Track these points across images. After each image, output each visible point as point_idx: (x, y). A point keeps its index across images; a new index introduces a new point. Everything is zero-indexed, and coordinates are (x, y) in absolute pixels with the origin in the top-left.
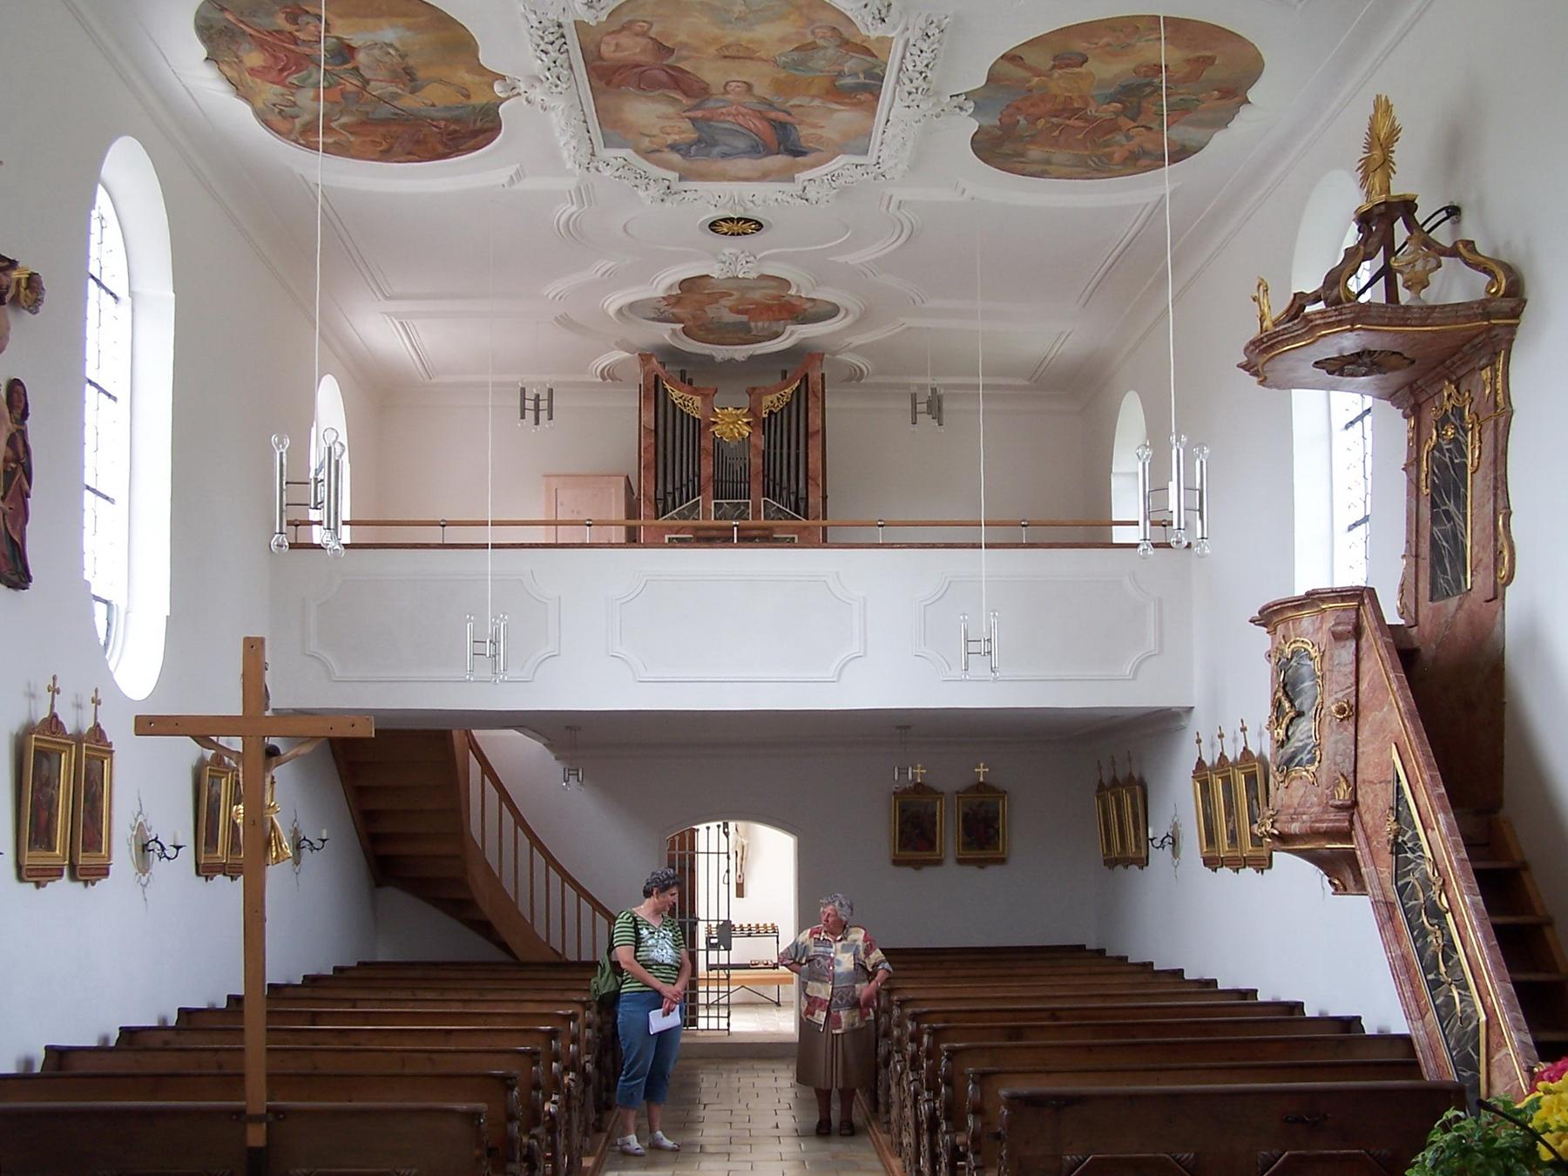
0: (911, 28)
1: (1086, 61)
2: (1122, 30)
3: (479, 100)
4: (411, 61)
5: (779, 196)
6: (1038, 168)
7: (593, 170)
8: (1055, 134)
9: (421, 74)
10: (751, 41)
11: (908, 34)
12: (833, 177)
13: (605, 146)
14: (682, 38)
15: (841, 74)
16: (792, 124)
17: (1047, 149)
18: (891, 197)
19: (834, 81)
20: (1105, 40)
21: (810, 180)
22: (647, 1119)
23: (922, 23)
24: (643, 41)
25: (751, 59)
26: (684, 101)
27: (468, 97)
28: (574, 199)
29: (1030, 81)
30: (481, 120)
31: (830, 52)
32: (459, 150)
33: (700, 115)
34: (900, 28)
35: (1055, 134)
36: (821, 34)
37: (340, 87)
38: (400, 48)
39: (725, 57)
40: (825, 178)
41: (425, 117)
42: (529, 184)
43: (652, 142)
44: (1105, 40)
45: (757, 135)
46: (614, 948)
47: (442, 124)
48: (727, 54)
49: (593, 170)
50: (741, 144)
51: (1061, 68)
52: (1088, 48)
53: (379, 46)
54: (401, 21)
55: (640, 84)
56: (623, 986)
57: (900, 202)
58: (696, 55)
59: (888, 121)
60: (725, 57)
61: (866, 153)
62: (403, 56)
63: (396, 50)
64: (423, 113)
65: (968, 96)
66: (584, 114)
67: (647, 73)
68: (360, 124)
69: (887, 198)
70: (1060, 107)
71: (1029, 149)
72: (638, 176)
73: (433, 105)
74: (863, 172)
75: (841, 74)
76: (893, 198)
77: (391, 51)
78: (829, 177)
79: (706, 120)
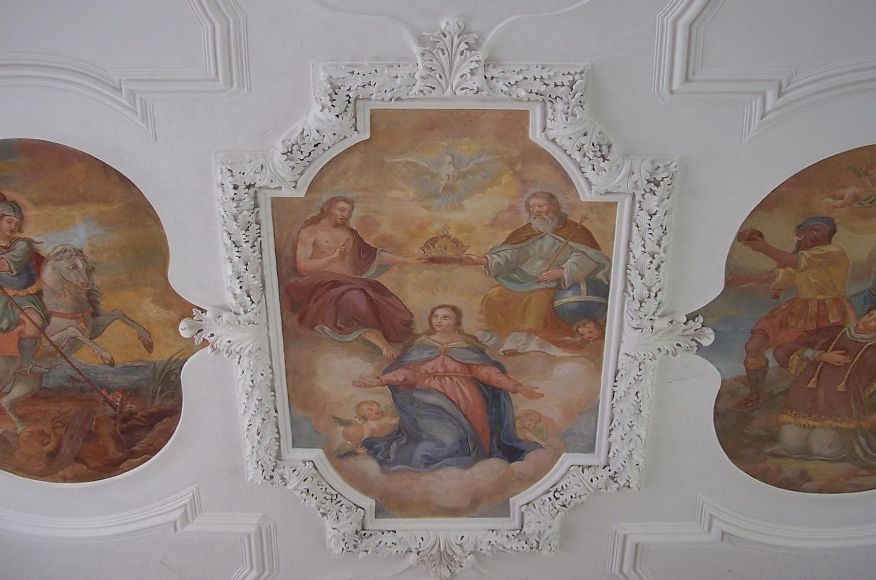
0: (636, 171)
1: (833, 231)
2: (866, 173)
3: (161, 355)
4: (98, 280)
5: (492, 537)
6: (791, 468)
7: (277, 478)
8: (811, 385)
9: (106, 304)
10: (461, 228)
11: (634, 177)
12: (555, 491)
13: (293, 447)
14: (385, 228)
15: (559, 286)
16: (506, 392)
17: (804, 422)
18: (625, 537)
19: (552, 301)
20: (852, 190)
21: (528, 504)
22: (53, 341)
23: (647, 166)
24: (342, 236)
25: (460, 261)
26: (384, 350)
27: (149, 347)
28: (255, 563)
29: (774, 279)
30: (161, 393)
31: (548, 241)
32: (133, 455)
33: (401, 379)
34: (625, 170)
35: (811, 385)
36: (537, 208)
37: (13, 275)
38: (90, 258)
39: (432, 260)
40: (546, 497)
41: (102, 387)
42: (203, 524)
43: (346, 435)
44: (852, 190)
45: (465, 416)
46: (260, 253)
47: (118, 399)
48: (434, 254)
49: (277, 478)
50: (447, 435)
51: (807, 248)
52: (835, 207)
53: (68, 253)
54: (92, 208)
55: (335, 322)
56: (613, 572)
57: (637, 545)
58: (399, 258)
59: (617, 372)
60: (432, 260)
61: (590, 448)
62: (90, 271)
63: (85, 261)
64: (100, 378)
65: (703, 311)
66: (272, 373)
67: (345, 297)
68: (32, 398)
69: (621, 539)
70: (812, 326)
71: (785, 423)
72: (329, 497)
73: (112, 364)
74: (591, 476)
75: (559, 286)
76: (628, 540)
77: (80, 264)
78: (551, 495)
79: (410, 386)
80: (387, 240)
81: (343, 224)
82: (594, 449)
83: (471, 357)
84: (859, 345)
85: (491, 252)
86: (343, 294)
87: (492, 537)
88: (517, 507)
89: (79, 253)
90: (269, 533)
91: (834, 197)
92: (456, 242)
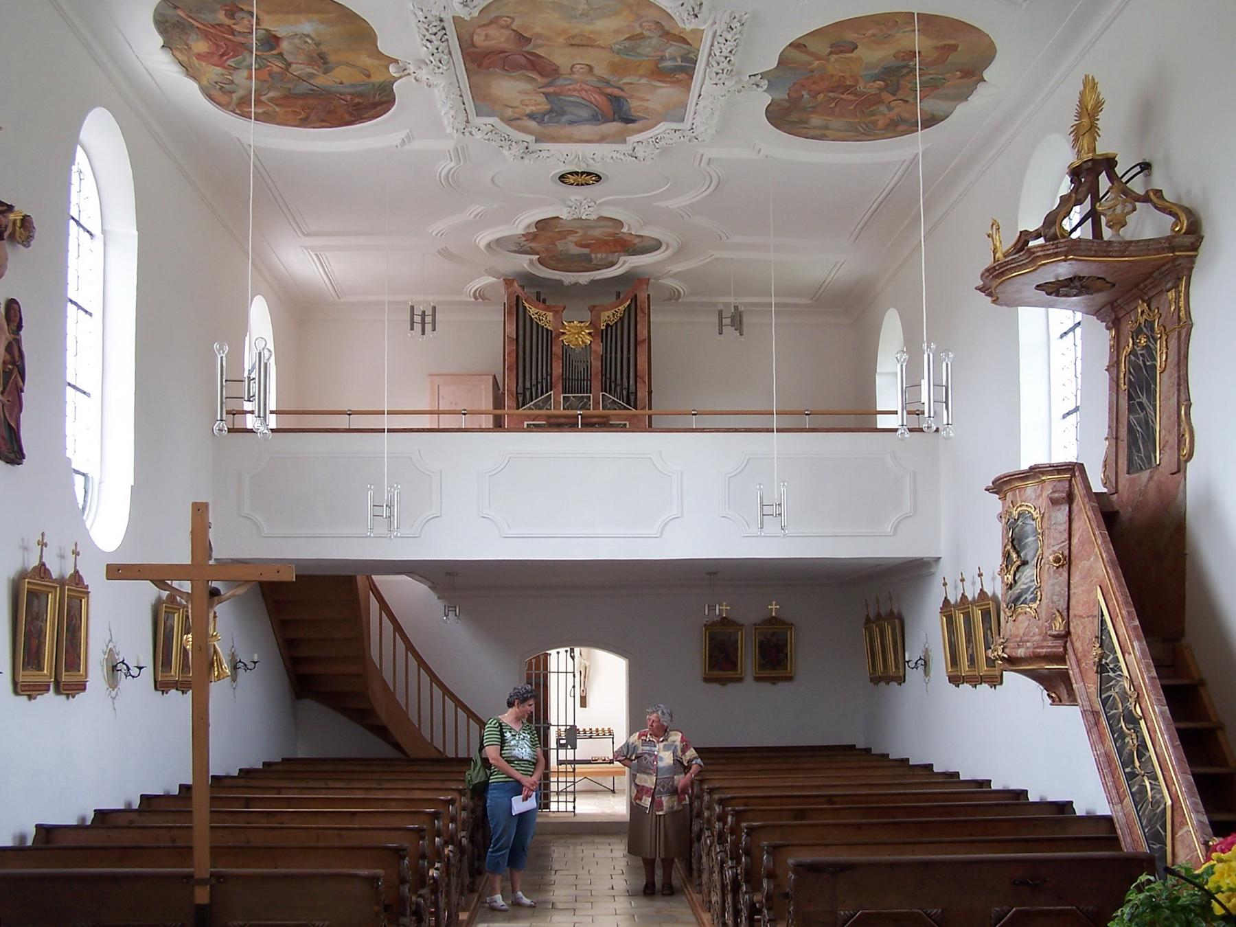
0: (718, 22)
2: (884, 24)
3: (377, 79)
4: (324, 48)
5: (614, 155)
6: (818, 132)
7: (467, 134)
8: (831, 106)
9: (332, 58)
10: (592, 32)
11: (716, 26)
12: (657, 139)
13: (477, 115)
14: (538, 30)
15: (663, 59)
16: (624, 98)
17: (825, 118)
18: (702, 155)
19: (657, 64)
20: (871, 32)
21: (638, 142)
23: (726, 18)
24: (507, 32)
25: (592, 46)
26: (539, 80)
27: (369, 76)
28: (453, 157)
29: (812, 64)
30: (379, 94)
31: (655, 41)
32: (362, 119)
33: (552, 91)
35: (831, 106)
37: (268, 68)
39: (572, 45)
40: (650, 140)
41: (335, 92)
42: (417, 145)
43: (514, 112)
44: (871, 32)
45: (597, 107)
46: (484, 747)
48: (573, 42)
49: (467, 134)
50: (584, 113)
51: (836, 53)
52: (858, 38)
53: (299, 36)
54: (316, 17)
55: (504, 66)
57: (710, 159)
58: (549, 43)
59: (700, 95)
60: (572, 45)
61: (682, 120)
62: (318, 44)
63: (313, 39)
64: (334, 89)
66: (460, 90)
67: (510, 57)
68: (284, 97)
69: (699, 156)
71: (812, 118)
72: (503, 139)
73: (342, 83)
74: (680, 135)
75: (663, 59)
76: (704, 156)
77: (308, 40)
78: (654, 140)
79: (557, 94)
80: (539, 36)
81: (507, 27)
82: (684, 120)
83: (600, 85)
84: (864, 93)
85: (614, 44)
86: (509, 56)
87: (614, 155)
88: (631, 143)
89: (308, 36)
90: (462, 148)
91: (859, 34)
92: (590, 38)
